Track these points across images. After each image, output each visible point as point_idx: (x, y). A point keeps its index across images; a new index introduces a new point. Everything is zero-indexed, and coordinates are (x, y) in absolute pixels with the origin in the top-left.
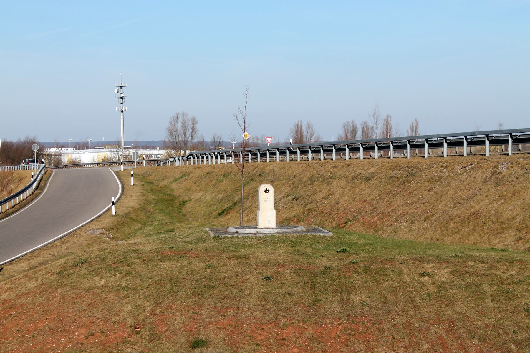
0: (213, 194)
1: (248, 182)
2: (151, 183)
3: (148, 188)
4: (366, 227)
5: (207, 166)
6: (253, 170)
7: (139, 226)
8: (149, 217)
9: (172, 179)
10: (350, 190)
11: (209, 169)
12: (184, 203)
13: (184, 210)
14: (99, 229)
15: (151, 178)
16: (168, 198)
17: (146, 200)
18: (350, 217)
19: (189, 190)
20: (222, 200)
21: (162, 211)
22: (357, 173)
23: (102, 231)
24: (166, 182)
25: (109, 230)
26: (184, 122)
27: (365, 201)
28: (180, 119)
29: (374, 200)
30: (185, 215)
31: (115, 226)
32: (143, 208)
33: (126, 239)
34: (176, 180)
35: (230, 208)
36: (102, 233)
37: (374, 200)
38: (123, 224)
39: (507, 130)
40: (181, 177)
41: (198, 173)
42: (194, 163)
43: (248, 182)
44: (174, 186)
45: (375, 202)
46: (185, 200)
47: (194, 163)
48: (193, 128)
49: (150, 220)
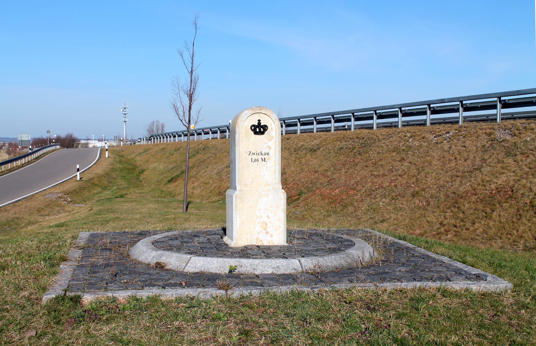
0: (166, 165)
1: (194, 155)
2: (123, 156)
3: (118, 159)
4: (327, 201)
5: (163, 144)
6: (198, 146)
7: (99, 190)
8: (111, 183)
9: (137, 154)
10: (295, 161)
11: (164, 146)
12: (142, 171)
13: (142, 177)
14: (58, 193)
15: (123, 153)
16: (131, 167)
17: (112, 169)
18: (302, 189)
19: (148, 161)
20: (172, 169)
21: (123, 177)
22: (299, 145)
23: (60, 195)
24: (133, 156)
25: (68, 194)
26: (157, 126)
27: (316, 172)
28: (155, 124)
29: (328, 170)
30: (141, 181)
31: (74, 191)
32: (107, 175)
33: (83, 202)
34: (140, 154)
35: (178, 176)
36: (59, 197)
37: (328, 170)
38: (84, 188)
39: (496, 94)
40: (144, 152)
41: (156, 148)
42: (154, 142)
43: (194, 155)
44: (138, 158)
45: (329, 173)
46: (143, 169)
47: (154, 142)
48: (162, 129)
49: (110, 185)
